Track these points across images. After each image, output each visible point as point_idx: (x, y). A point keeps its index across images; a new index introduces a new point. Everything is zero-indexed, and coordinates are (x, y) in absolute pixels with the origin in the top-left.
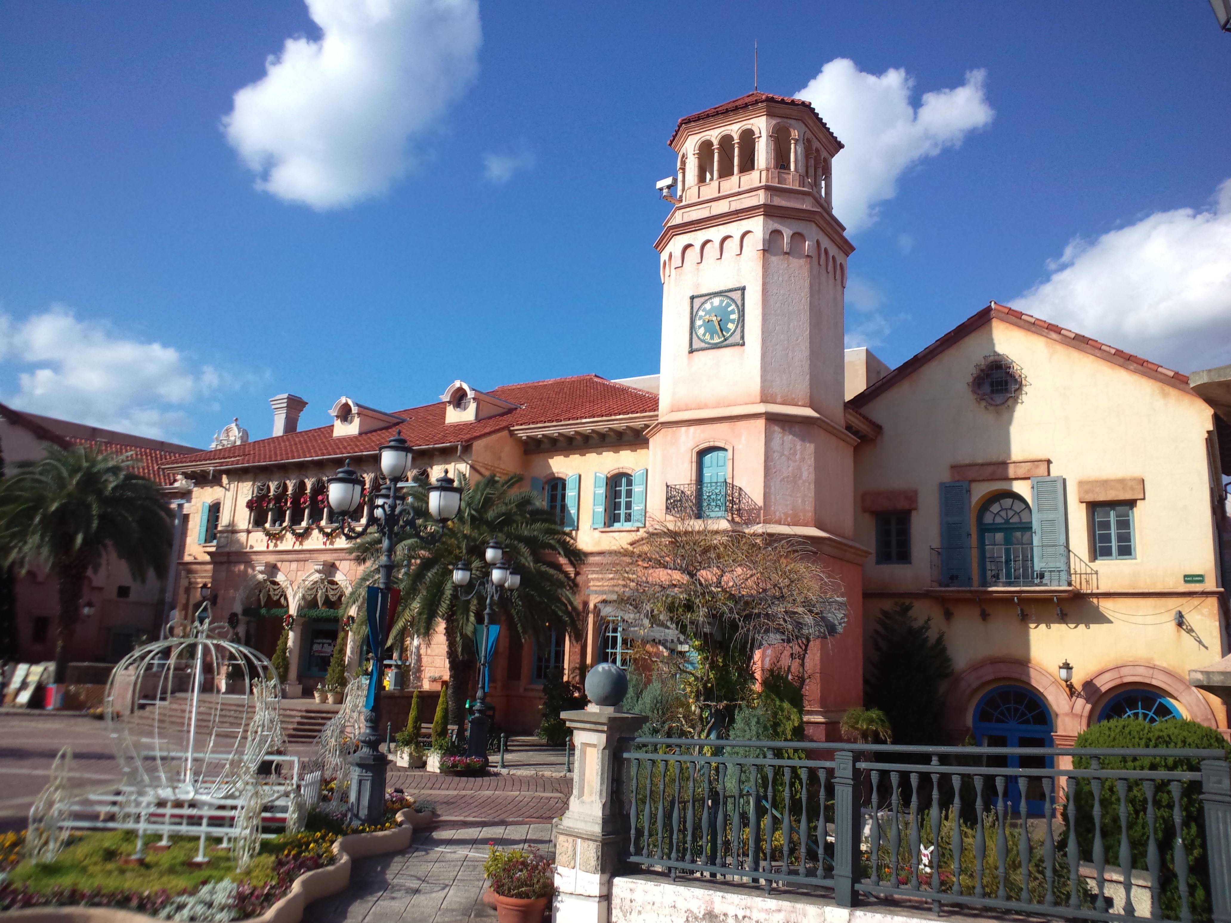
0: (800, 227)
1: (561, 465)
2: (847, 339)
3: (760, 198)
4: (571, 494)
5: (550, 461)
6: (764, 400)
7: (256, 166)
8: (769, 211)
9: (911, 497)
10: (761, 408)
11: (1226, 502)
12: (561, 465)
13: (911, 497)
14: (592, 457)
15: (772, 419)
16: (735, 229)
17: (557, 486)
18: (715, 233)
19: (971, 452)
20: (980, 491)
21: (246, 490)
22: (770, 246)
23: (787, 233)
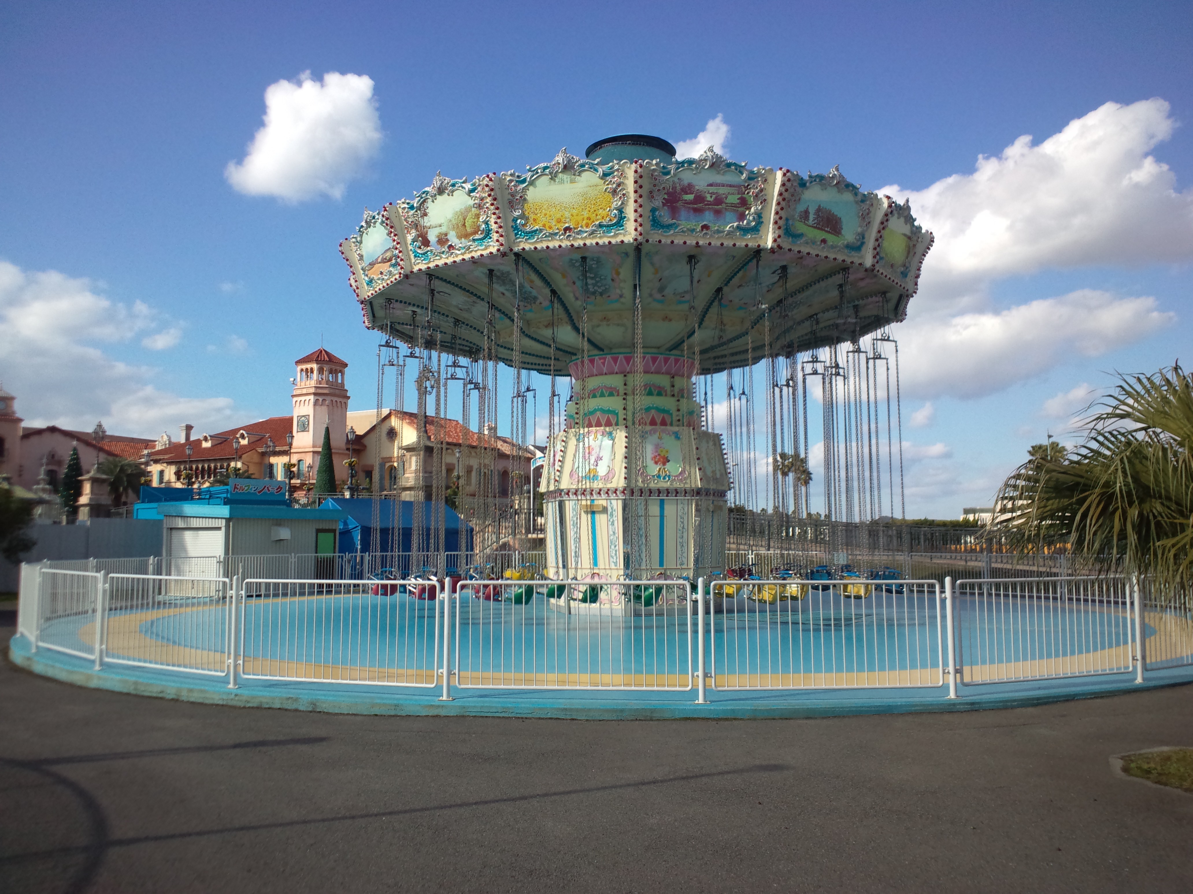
0: (324, 397)
1: (273, 460)
2: (1165, 167)
3: (312, 390)
4: (275, 469)
5: (1005, 222)
6: (313, 447)
7: (1004, 156)
8: (315, 394)
9: (372, 466)
10: (311, 450)
11: (911, 299)
12: (273, 460)
13: (372, 466)
14: (281, 457)
15: (314, 452)
16: (307, 398)
17: (271, 466)
18: (303, 398)
19: (385, 454)
20: (387, 465)
21: (173, 469)
22: (316, 403)
23: (321, 399)
